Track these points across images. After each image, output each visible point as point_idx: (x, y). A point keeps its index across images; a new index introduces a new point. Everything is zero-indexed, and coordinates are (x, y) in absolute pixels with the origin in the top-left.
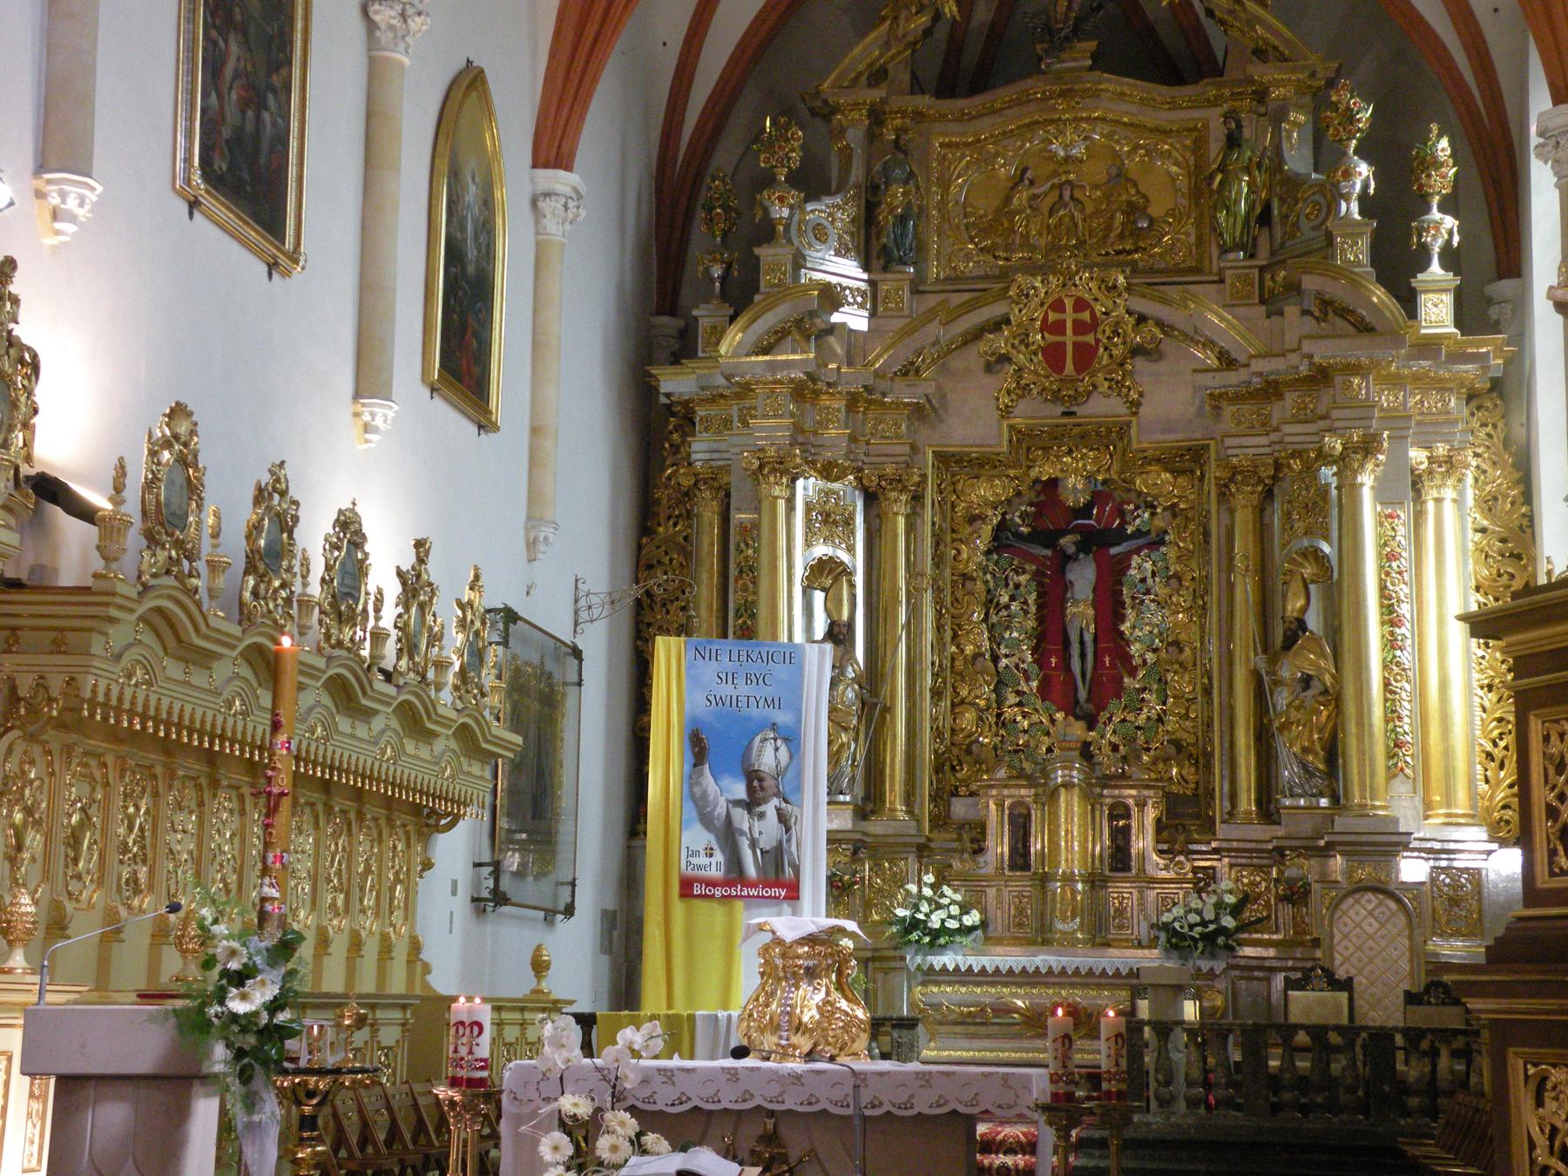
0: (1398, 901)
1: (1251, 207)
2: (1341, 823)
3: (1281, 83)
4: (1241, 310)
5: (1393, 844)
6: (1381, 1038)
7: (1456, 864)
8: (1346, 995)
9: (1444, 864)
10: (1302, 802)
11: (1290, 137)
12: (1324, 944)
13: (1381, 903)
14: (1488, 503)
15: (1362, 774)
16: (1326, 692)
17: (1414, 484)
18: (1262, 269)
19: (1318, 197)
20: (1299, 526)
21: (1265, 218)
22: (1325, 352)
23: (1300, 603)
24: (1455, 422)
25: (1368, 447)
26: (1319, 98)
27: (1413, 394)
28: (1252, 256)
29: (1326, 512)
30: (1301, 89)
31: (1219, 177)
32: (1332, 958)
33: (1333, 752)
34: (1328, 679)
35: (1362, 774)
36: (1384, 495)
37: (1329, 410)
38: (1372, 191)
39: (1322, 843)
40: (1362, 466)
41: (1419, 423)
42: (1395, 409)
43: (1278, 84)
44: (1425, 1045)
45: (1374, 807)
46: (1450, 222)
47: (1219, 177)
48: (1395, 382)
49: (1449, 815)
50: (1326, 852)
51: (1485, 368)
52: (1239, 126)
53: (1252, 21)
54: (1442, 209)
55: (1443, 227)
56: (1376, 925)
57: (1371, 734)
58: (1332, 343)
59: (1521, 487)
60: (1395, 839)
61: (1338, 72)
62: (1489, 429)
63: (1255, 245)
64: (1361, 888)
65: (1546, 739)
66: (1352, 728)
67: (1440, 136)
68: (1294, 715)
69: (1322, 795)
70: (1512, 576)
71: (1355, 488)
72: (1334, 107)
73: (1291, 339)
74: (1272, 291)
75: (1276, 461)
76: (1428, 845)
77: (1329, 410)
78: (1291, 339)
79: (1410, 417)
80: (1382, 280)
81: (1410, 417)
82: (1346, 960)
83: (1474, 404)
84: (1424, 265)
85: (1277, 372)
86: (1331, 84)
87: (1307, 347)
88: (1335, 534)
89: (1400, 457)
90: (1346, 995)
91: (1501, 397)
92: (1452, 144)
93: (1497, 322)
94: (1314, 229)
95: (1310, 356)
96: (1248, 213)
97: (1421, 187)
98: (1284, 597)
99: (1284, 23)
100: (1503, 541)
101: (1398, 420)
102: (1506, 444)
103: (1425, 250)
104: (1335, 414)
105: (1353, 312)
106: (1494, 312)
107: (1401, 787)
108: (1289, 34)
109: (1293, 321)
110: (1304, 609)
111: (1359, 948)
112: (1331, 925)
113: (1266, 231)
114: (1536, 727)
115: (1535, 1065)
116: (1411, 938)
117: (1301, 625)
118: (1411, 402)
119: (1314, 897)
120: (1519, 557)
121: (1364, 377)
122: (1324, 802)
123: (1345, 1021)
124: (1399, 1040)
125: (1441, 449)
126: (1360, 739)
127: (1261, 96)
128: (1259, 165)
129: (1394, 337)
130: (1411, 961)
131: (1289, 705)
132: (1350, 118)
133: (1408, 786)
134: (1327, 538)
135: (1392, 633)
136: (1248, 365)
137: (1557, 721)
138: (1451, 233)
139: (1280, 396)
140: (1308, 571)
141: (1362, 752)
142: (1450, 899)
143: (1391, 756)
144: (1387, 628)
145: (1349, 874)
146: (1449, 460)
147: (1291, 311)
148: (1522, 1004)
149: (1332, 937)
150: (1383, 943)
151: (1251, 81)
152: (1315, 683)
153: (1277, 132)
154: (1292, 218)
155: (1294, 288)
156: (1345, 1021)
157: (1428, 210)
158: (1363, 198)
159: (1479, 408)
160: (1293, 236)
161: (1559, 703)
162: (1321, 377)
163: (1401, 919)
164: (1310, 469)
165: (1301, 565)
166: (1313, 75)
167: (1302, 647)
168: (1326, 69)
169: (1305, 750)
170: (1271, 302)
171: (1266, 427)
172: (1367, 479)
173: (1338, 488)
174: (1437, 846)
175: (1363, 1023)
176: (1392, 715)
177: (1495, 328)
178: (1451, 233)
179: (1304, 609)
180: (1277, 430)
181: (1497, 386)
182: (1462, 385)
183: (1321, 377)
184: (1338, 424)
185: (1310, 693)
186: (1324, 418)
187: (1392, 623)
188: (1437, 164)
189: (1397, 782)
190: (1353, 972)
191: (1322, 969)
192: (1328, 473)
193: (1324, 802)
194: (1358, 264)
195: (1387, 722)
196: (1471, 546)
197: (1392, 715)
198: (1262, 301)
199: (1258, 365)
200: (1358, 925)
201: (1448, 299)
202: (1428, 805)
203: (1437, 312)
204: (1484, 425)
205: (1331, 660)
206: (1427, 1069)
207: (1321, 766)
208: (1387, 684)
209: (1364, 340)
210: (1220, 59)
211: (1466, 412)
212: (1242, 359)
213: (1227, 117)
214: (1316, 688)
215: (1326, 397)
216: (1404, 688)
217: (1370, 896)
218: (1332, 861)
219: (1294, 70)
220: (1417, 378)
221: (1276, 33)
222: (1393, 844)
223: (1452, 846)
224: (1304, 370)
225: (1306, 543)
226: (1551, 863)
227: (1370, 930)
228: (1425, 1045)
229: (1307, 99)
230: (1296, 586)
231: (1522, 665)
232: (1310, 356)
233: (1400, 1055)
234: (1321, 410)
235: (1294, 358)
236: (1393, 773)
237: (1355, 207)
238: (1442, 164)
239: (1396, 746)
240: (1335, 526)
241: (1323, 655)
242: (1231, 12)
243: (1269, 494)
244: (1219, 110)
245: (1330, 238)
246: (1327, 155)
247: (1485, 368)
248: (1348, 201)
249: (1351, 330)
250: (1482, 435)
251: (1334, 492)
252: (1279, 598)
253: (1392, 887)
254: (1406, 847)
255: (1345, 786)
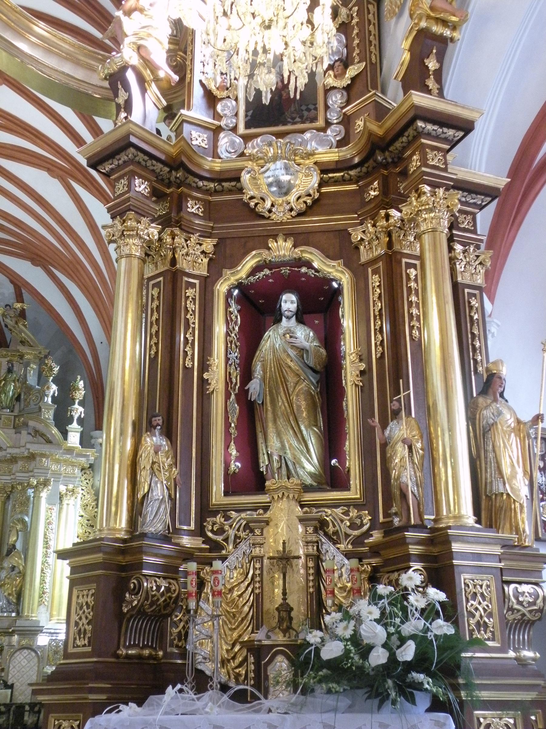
0: (36, 652)
1: (13, 395)
2: (18, 623)
3: (29, 354)
4: (5, 430)
5: (35, 630)
6: (20, 707)
7: (58, 638)
8: (10, 691)
9: (54, 638)
10: (5, 614)
11: (30, 372)
12: (6, 670)
13: (29, 654)
14: (85, 507)
15: (29, 603)
16: (20, 572)
17: (60, 498)
18: (15, 417)
19: (38, 394)
20: (18, 510)
21: (18, 399)
22: (34, 448)
23: (15, 538)
24: (76, 477)
25: (46, 484)
26: (41, 361)
27: (63, 466)
28: (12, 411)
29: (27, 505)
30: (36, 356)
31: (3, 382)
32: (8, 676)
33: (19, 595)
34: (21, 568)
35: (29, 603)
36: (50, 501)
37: (33, 469)
38: (56, 395)
39: (11, 630)
40: (43, 490)
41: (64, 477)
42: (56, 471)
43: (28, 354)
44: (36, 709)
45: (32, 617)
46: (81, 409)
47: (3, 382)
48: (58, 461)
49: (58, 620)
50: (12, 634)
51: (88, 460)
52: (13, 366)
53: (21, 331)
54: (80, 404)
55: (78, 411)
56: (26, 662)
57: (34, 589)
58: (36, 445)
59: (96, 502)
60: (38, 629)
61: (49, 353)
62: (87, 481)
63: (14, 408)
64: (23, 648)
65: (78, 597)
66: (28, 586)
67: (80, 380)
68: (7, 580)
69: (13, 612)
70: (90, 533)
71: (39, 498)
72: (46, 365)
73: (22, 443)
74: (18, 424)
75: (12, 485)
76: (49, 631)
77: (33, 469)
78: (22, 443)
79: (61, 474)
80: (56, 426)
81: (61, 474)
82: (13, 676)
83: (83, 472)
84: (71, 422)
85: (17, 454)
86: (46, 357)
87: (28, 446)
88: (30, 514)
89: (56, 488)
90: (10, 691)
91: (93, 470)
92: (84, 383)
93: (94, 445)
94: (35, 405)
95: (29, 449)
96: (12, 397)
97: (73, 396)
98: (9, 535)
99: (33, 335)
100: (88, 520)
101: (57, 475)
102: (92, 486)
103: (72, 417)
104: (35, 471)
105: (45, 435)
106: (93, 441)
107: (42, 609)
108: (32, 337)
109: (24, 436)
110: (16, 541)
111: (18, 672)
112: (9, 663)
113: (18, 403)
114: (75, 592)
115: (58, 720)
116: (38, 667)
117: (14, 547)
118: (62, 469)
119: (4, 652)
120: (93, 526)
121: (47, 458)
122: (14, 614)
123: (8, 701)
124: (27, 708)
125: (71, 487)
126: (30, 590)
127: (21, 357)
128: (18, 380)
129: (59, 446)
130: (37, 676)
131: (5, 577)
132: (51, 369)
133: (45, 609)
134: (27, 515)
135: (46, 551)
136: (6, 450)
137: (82, 591)
138: (81, 413)
139: (16, 462)
140: (19, 527)
141: (30, 596)
142: (55, 651)
143: (40, 597)
144: (45, 550)
145: (19, 642)
146: (73, 491)
147: (24, 432)
148: (56, 697)
149: (9, 667)
150: (28, 669)
151: (19, 351)
152: (16, 569)
153: (26, 370)
154: (28, 400)
155: (26, 425)
156: (8, 701)
157: (74, 404)
158: (53, 397)
159: (85, 473)
160: (27, 406)
161: (84, 584)
162: (32, 457)
163: (36, 660)
164: (24, 490)
165: (17, 524)
166: (40, 353)
167: (13, 555)
168: (44, 352)
169: (9, 594)
170: (17, 428)
171: (10, 473)
172: (44, 495)
173: (34, 497)
174: (52, 631)
175: (15, 702)
176: (43, 581)
177: (92, 446)
178: (81, 413)
179: (16, 541)
180: (13, 474)
181: (91, 466)
182: (80, 465)
183: (32, 457)
184: (36, 474)
185: (14, 572)
186: (31, 472)
187: (47, 548)
188: (79, 389)
189: (41, 607)
190: (15, 681)
191: (3, 681)
192: (30, 492)
193: (14, 614)
194: (49, 419)
195: (41, 584)
196: (77, 522)
197: (43, 581)
198: (14, 428)
199: (9, 450)
200: (20, 662)
201: (78, 435)
202: (51, 616)
203: (74, 439)
204: (86, 479)
205: (23, 560)
206: (36, 719)
207: (14, 601)
208: (42, 570)
209: (48, 446)
210: (8, 342)
211: (80, 475)
212: (4, 447)
213: (8, 362)
214: (17, 570)
215: (33, 464)
216: (48, 572)
217: (26, 651)
218: (13, 637)
219: (33, 350)
220: (65, 461)
221: (28, 336)
222: (35, 630)
223: (58, 631)
224: (26, 454)
225: (19, 516)
226: (74, 642)
227: (24, 664)
228: (36, 709)
229: (37, 361)
230: (14, 532)
231: (74, 570)
232: (29, 449)
233: (27, 714)
234: (31, 469)
235: (23, 449)
236: (40, 603)
237: (50, 399)
238: (80, 390)
239: (43, 593)
240: (31, 511)
241: (20, 558)
242: (14, 327)
243: (8, 498)
244: (6, 359)
245: (40, 409)
246: (42, 379)
247: (88, 460)
248: (47, 397)
249: (44, 442)
250: (85, 483)
251: (32, 499)
252: (7, 536)
253: (34, 647)
254: (41, 631)
255: (22, 609)
